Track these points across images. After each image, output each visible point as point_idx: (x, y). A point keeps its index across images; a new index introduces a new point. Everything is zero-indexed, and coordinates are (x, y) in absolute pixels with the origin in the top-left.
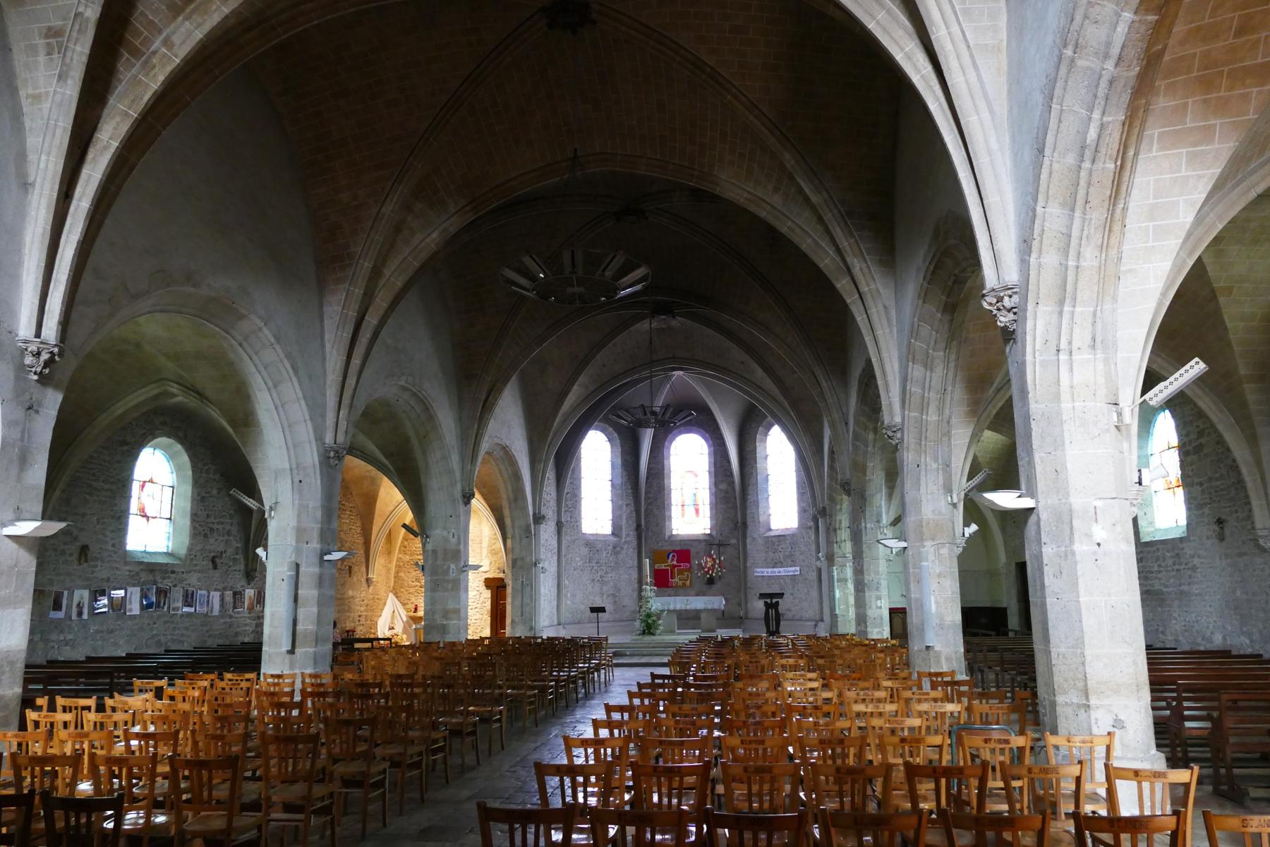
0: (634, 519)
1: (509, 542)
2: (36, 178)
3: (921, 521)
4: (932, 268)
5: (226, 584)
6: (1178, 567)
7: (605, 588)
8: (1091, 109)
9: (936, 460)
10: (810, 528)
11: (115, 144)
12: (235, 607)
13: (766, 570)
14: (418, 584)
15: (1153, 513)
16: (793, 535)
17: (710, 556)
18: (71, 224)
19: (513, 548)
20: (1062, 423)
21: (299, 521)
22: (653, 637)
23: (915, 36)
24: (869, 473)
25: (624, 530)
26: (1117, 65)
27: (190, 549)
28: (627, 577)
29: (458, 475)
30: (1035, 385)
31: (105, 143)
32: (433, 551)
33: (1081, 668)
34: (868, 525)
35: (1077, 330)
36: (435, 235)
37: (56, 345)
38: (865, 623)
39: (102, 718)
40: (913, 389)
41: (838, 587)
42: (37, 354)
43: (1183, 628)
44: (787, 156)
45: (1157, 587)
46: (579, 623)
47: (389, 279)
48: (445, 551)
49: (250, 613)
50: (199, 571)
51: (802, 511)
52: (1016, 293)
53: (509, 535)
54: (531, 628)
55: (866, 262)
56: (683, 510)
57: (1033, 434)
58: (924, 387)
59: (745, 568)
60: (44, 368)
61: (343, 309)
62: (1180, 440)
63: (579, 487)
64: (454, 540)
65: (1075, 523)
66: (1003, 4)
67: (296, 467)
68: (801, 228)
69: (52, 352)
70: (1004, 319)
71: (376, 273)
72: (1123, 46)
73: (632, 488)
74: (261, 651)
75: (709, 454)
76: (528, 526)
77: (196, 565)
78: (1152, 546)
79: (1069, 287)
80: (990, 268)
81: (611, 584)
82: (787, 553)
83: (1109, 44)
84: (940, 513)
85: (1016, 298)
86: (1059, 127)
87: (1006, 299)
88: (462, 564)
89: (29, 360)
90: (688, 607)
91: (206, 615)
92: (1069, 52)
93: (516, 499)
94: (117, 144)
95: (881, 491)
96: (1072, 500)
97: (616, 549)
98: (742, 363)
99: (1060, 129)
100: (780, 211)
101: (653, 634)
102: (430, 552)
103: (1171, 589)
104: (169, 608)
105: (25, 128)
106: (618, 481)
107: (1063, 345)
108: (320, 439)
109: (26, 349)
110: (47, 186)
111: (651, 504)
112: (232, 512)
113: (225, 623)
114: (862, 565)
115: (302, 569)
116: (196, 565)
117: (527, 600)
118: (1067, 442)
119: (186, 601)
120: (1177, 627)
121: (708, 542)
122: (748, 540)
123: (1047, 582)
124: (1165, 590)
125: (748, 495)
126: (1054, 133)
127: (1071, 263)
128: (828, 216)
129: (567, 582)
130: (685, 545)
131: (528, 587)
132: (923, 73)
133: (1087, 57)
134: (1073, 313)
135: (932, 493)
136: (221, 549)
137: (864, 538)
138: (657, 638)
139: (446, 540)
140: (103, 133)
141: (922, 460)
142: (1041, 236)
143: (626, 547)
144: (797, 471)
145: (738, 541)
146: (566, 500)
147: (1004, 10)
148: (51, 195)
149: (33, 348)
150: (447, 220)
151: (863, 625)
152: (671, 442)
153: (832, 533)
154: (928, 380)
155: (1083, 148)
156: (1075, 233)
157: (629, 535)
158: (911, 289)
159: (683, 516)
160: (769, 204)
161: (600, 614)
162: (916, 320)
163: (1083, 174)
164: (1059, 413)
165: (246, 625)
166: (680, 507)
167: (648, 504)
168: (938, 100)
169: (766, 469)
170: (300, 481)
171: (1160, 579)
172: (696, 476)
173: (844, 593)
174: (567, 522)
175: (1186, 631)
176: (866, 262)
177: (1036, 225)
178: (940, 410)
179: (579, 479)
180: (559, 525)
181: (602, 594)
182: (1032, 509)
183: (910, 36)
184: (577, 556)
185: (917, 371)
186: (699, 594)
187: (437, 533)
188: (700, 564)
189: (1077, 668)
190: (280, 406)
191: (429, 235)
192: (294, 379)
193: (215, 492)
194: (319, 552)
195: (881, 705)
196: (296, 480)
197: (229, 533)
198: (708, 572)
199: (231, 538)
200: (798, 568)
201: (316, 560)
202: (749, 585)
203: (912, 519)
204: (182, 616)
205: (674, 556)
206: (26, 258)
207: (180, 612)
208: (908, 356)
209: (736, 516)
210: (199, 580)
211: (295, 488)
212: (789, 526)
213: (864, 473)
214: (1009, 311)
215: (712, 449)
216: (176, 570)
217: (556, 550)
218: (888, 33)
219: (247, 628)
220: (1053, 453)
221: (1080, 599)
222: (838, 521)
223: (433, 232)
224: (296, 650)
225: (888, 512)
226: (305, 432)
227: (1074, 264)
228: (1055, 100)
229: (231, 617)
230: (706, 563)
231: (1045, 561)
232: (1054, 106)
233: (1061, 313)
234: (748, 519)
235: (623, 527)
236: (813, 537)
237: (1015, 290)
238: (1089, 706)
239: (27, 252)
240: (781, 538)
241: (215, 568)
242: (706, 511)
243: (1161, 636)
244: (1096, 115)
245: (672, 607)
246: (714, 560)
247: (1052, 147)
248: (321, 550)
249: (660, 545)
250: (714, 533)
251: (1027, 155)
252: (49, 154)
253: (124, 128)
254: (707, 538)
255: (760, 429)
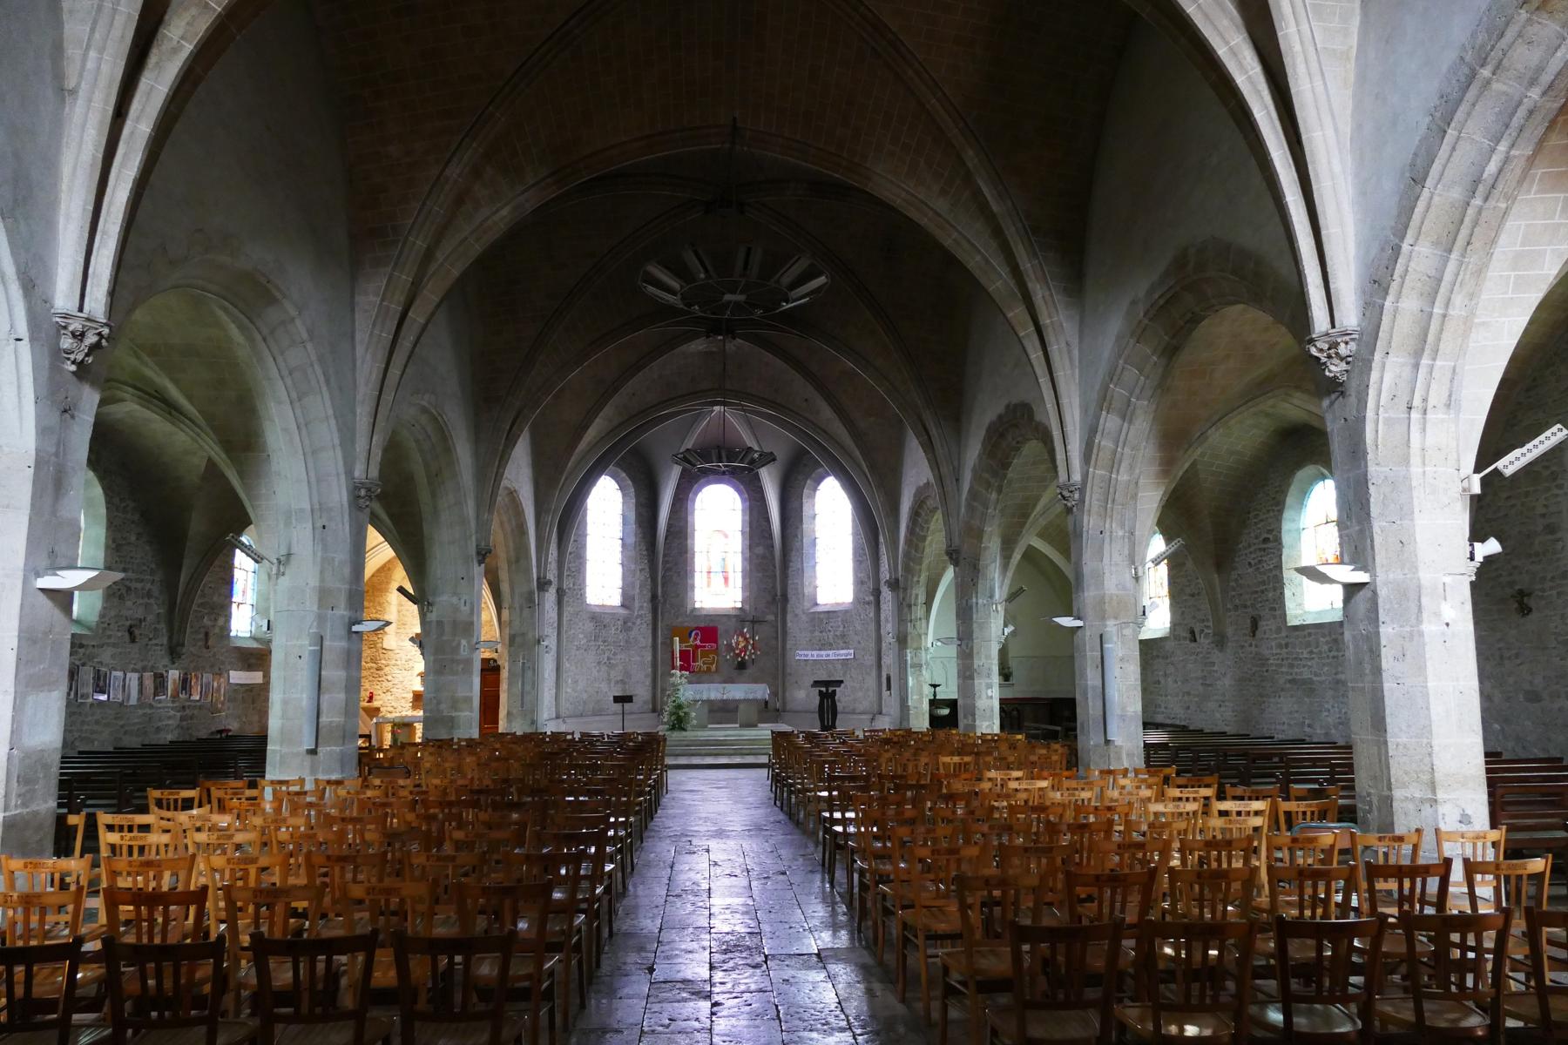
0: (649, 587)
1: (505, 614)
2: (79, 84)
3: (1103, 597)
4: (1162, 302)
5: (145, 663)
6: (1336, 654)
7: (613, 673)
8: (1497, 140)
9: (1122, 526)
10: (868, 603)
11: (188, 48)
12: (156, 694)
13: (809, 653)
14: (374, 665)
15: (1302, 594)
16: (846, 612)
17: (743, 635)
18: (125, 154)
19: (511, 621)
20: (1410, 488)
21: (322, 580)
22: (684, 733)
23: (1243, 30)
24: (985, 539)
25: (636, 601)
26: (1544, 93)
27: (102, 616)
28: (638, 658)
29: (473, 524)
30: (1377, 446)
31: (175, 43)
32: (437, 622)
33: (1427, 760)
34: (980, 601)
35: (1434, 386)
36: (504, 212)
37: (106, 325)
38: (973, 715)
39: (218, 839)
40: (1102, 443)
41: (912, 674)
42: (79, 336)
43: (1338, 720)
44: (971, 153)
45: (1306, 675)
46: (582, 715)
47: (442, 264)
48: (455, 624)
49: (173, 702)
50: (114, 645)
51: (859, 583)
52: (1353, 340)
53: (506, 604)
54: (533, 722)
55: (1050, 289)
56: (709, 578)
57: (1372, 500)
58: (1118, 442)
59: (784, 648)
60: (87, 355)
61: (382, 300)
62: (1340, 516)
63: (584, 546)
64: (465, 609)
65: (1424, 601)
66: (1357, 5)
67: (320, 509)
68: (969, 241)
69: (99, 334)
70: (1335, 369)
71: (428, 256)
72: (1559, 74)
73: (647, 550)
74: (265, 751)
75: (743, 510)
76: (531, 593)
77: (109, 637)
78: (1304, 630)
79: (1431, 338)
80: (1320, 309)
81: (621, 668)
82: (838, 633)
83: (1540, 69)
84: (1124, 588)
85: (1353, 346)
86: (1450, 156)
87: (1343, 345)
88: (475, 640)
89: (67, 343)
90: (725, 697)
91: (121, 704)
92: (1486, 73)
93: (517, 561)
94: (191, 47)
95: (995, 561)
96: (1421, 574)
97: (627, 624)
98: (806, 400)
99: (1452, 159)
100: (944, 219)
101: (684, 730)
102: (434, 624)
103: (1323, 678)
104: (76, 694)
105: (62, 9)
106: (631, 540)
107: (1417, 402)
108: (349, 472)
109: (65, 328)
110: (98, 96)
111: (669, 569)
112: (153, 566)
113: (144, 714)
114: (972, 647)
115: (327, 643)
116: (109, 637)
117: (528, 688)
118: (1416, 510)
119: (98, 685)
120: (1330, 720)
121: (739, 618)
122: (789, 617)
123: (1384, 665)
124: (1315, 679)
125: (790, 561)
126: (1443, 162)
127: (1437, 310)
128: (1011, 233)
129: (568, 665)
130: (712, 621)
131: (528, 671)
132: (1251, 73)
133: (1507, 81)
134: (1432, 367)
135: (1117, 565)
136: (140, 614)
137: (974, 616)
138: (689, 735)
139: (456, 609)
140: (171, 28)
141: (1107, 526)
142: (1403, 278)
143: (638, 622)
144: (855, 534)
145: (776, 617)
146: (569, 563)
147: (1358, 11)
148: (105, 110)
149: (76, 326)
150: (523, 193)
151: (970, 718)
152: (696, 494)
153: (906, 610)
154: (1124, 433)
155: (1476, 182)
156: (1448, 277)
157: (643, 607)
158: (1114, 325)
159: (709, 585)
160: (932, 209)
161: (627, 706)
162: (1121, 362)
163: (1470, 211)
164: (1407, 478)
165: (169, 718)
166: (705, 575)
167: (666, 570)
168: (1266, 107)
169: (814, 531)
170: (324, 527)
171: (1310, 667)
172: (726, 536)
173: (918, 681)
174: (569, 589)
175: (1340, 724)
176: (1050, 289)
177: (1398, 264)
178: (1131, 468)
179: (585, 536)
180: (560, 593)
181: (609, 680)
182: (1363, 585)
183: (1237, 26)
184: (580, 632)
185: (1110, 422)
186: (730, 680)
187: (444, 600)
188: (729, 646)
189: (1421, 760)
190: (304, 425)
191: (497, 211)
192: (324, 389)
193: (133, 538)
194: (347, 620)
195: (1181, 804)
196: (319, 524)
197: (149, 595)
198: (739, 655)
199: (152, 601)
200: (852, 651)
201: (343, 632)
202: (788, 671)
203: (1092, 594)
204: (92, 705)
205: (697, 634)
206: (63, 196)
207: (90, 700)
208: (1102, 402)
209: (774, 587)
210: (113, 657)
211: (317, 536)
212: (840, 600)
213: (980, 541)
214: (1342, 359)
215: (748, 503)
216: (84, 642)
217: (556, 625)
218: (1212, 23)
219: (170, 722)
220: (1398, 522)
221: (1429, 684)
222: (913, 596)
223: (502, 208)
224: (319, 749)
225: (1001, 587)
226: (333, 460)
227: (1441, 312)
228: (1453, 125)
229: (151, 706)
230: (737, 643)
231: (1383, 642)
232: (1449, 131)
233: (1416, 366)
234: (789, 591)
235: (636, 597)
236: (872, 615)
237: (1353, 336)
238: (1436, 801)
239: (64, 187)
240: (831, 614)
241: (133, 640)
242: (737, 580)
243: (1307, 729)
244: (1502, 148)
245: (705, 698)
246: (746, 639)
247: (1437, 177)
248: (350, 618)
249: (680, 620)
250: (747, 607)
251: (1390, 185)
252: (101, 51)
253: (203, 25)
254: (737, 613)
255: (809, 481)
